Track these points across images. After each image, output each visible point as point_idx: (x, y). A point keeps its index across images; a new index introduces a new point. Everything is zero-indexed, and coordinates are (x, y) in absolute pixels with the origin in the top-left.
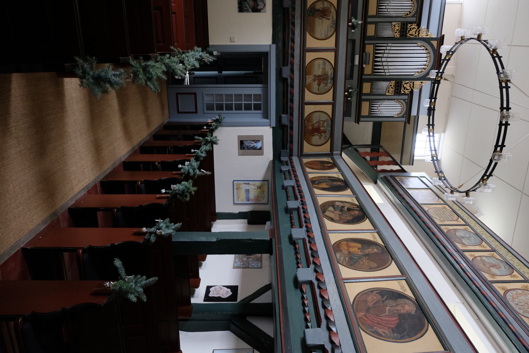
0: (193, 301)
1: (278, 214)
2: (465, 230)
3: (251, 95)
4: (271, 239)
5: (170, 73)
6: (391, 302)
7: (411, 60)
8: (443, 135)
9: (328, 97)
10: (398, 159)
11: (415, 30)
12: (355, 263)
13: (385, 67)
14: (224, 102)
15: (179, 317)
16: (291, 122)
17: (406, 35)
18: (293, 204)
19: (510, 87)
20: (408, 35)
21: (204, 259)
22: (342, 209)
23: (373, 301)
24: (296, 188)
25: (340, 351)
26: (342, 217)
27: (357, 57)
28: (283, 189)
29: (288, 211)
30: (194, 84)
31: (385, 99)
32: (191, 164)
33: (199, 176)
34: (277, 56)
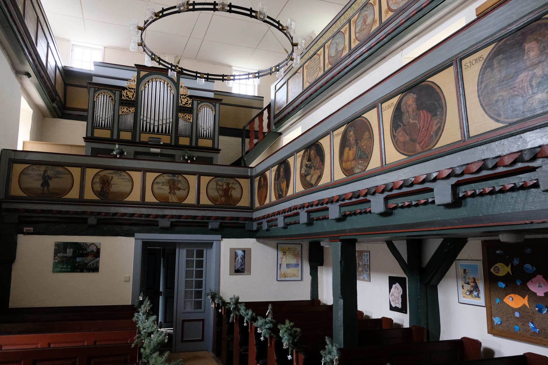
0: (406, 325)
1: (314, 233)
2: (329, 47)
3: (187, 261)
4: (341, 240)
5: (161, 348)
6: (405, 117)
7: (158, 98)
8: (234, 68)
9: (192, 180)
10: (256, 112)
11: (128, 93)
12: (365, 154)
13: (164, 122)
14: (193, 289)
15: (425, 340)
16: (217, 218)
17: (133, 101)
18: (303, 218)
19: (194, 2)
20: (133, 99)
21: (361, 313)
22: (309, 167)
23: (404, 136)
24: (287, 214)
25: (458, 168)
26: (317, 167)
27: (153, 150)
28: (287, 228)
29: (310, 223)
30: (173, 322)
31: (197, 123)
32: (261, 327)
33: (273, 318)
34: (147, 232)
